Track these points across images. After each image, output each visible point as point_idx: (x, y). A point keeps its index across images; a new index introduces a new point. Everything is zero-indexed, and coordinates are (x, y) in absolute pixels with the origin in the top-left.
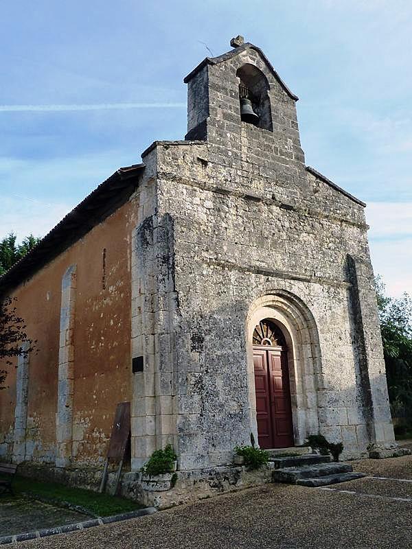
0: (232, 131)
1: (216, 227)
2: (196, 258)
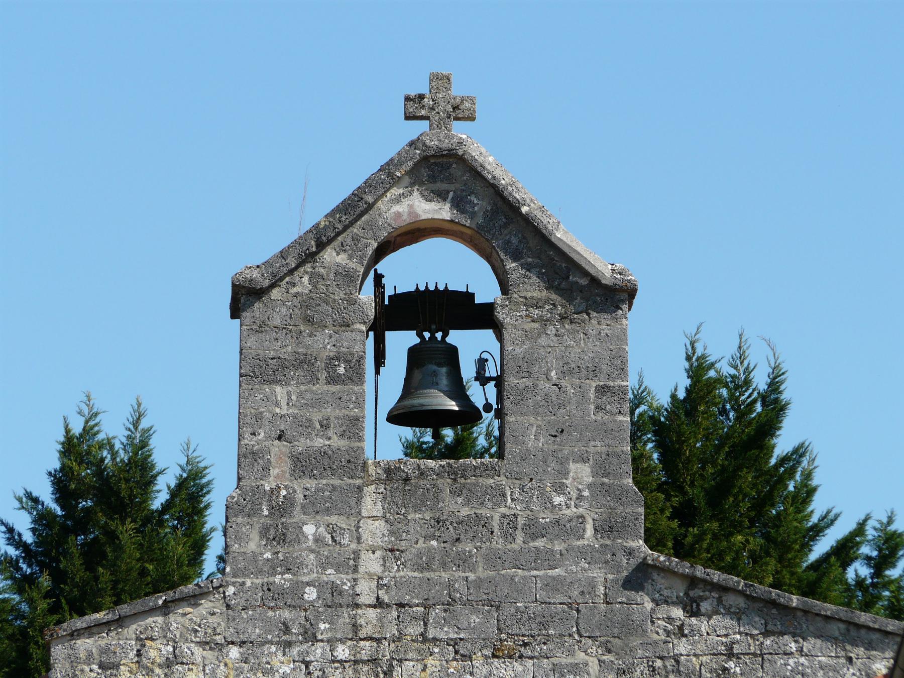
0: (328, 512)
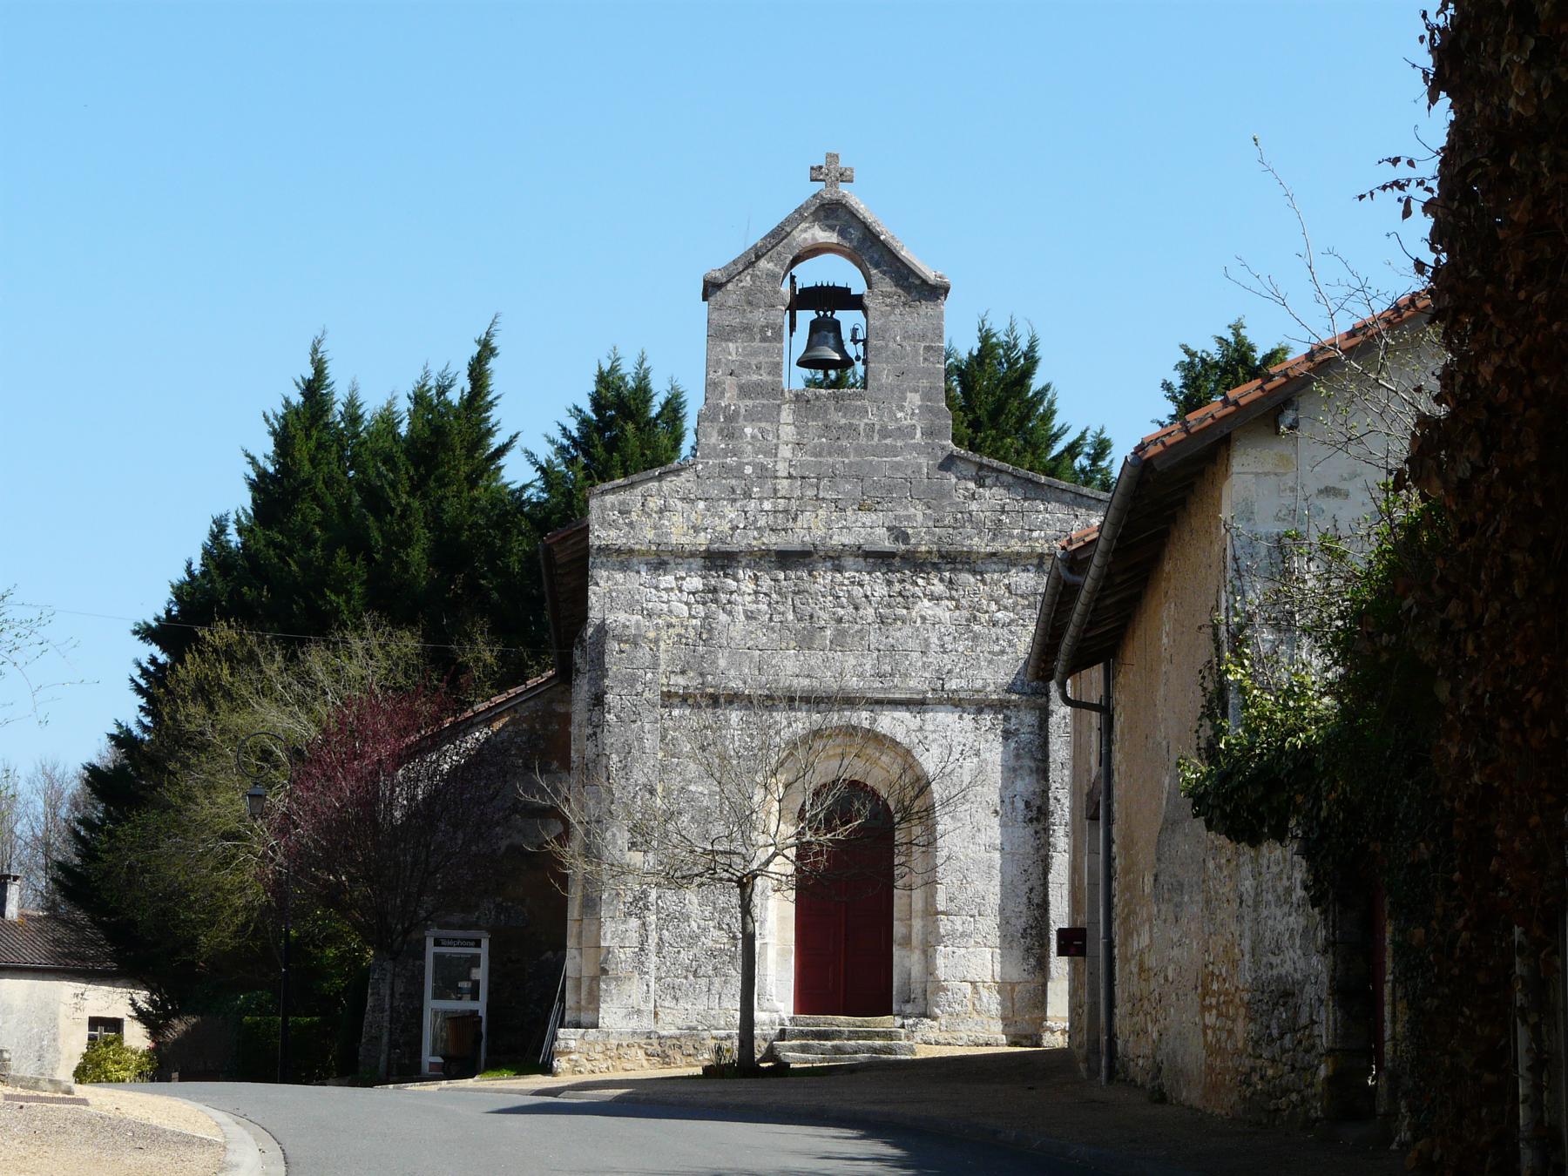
1: (707, 629)
2: (647, 695)
